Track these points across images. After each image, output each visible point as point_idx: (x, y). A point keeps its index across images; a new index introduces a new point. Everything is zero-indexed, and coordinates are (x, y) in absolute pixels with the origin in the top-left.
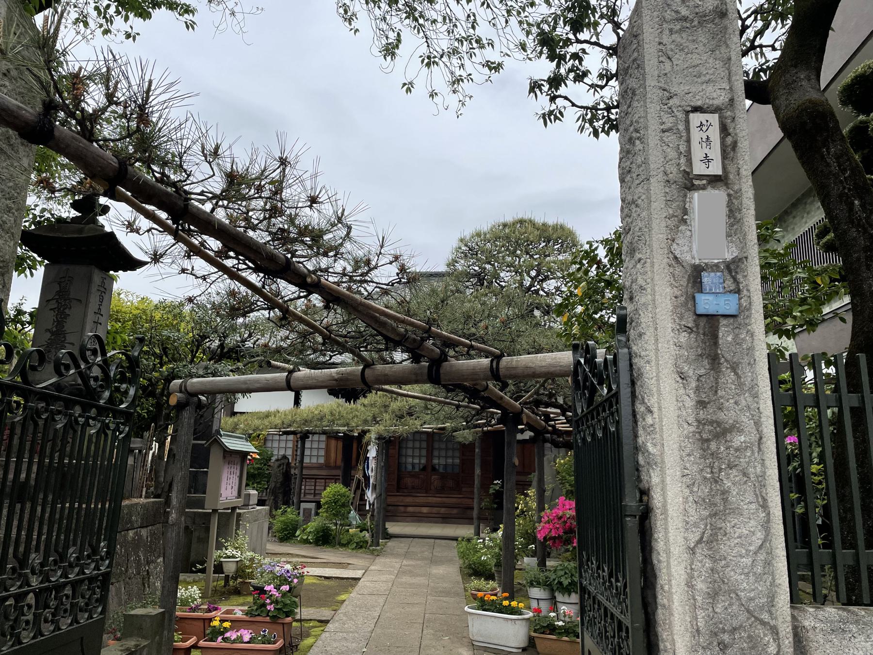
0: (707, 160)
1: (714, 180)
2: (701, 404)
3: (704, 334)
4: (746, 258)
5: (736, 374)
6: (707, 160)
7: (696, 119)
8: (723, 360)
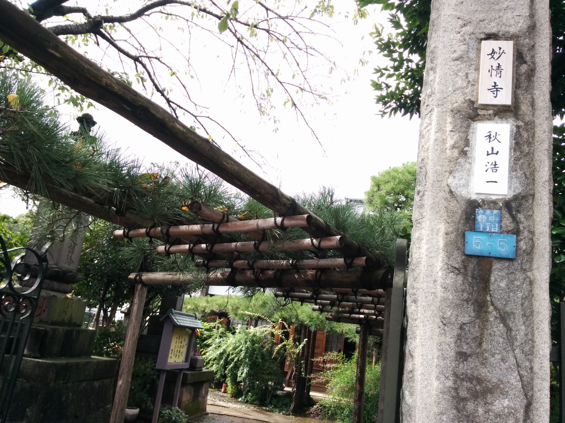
0: (496, 88)
1: (501, 112)
2: (462, 356)
3: (473, 277)
4: (533, 195)
5: (506, 325)
6: (496, 88)
7: (488, 46)
8: (491, 308)
